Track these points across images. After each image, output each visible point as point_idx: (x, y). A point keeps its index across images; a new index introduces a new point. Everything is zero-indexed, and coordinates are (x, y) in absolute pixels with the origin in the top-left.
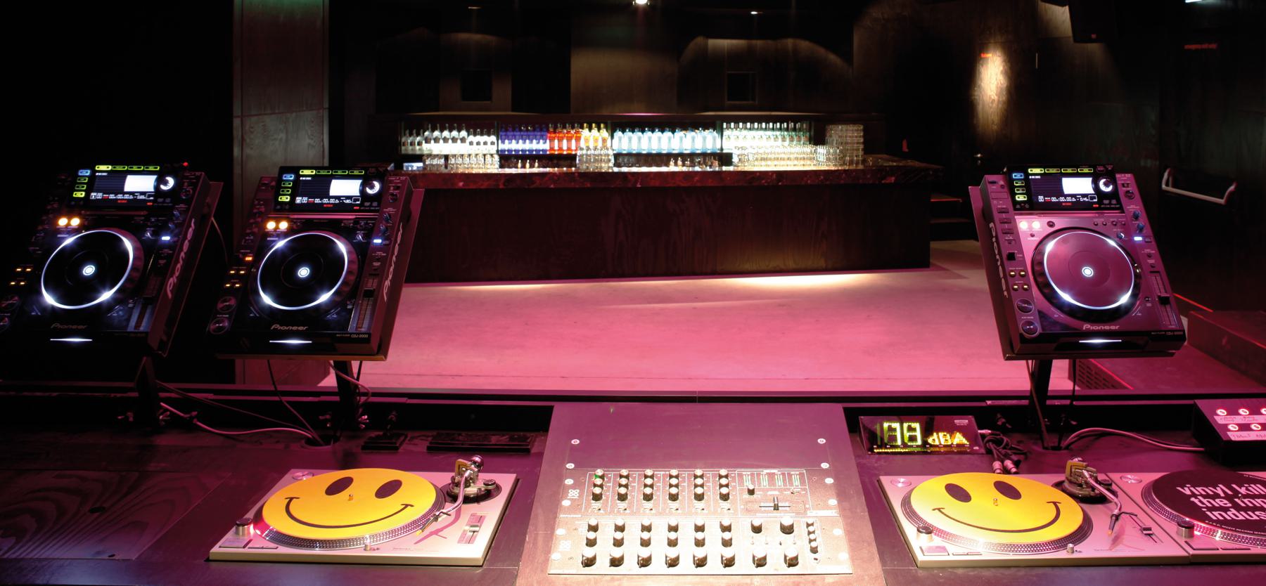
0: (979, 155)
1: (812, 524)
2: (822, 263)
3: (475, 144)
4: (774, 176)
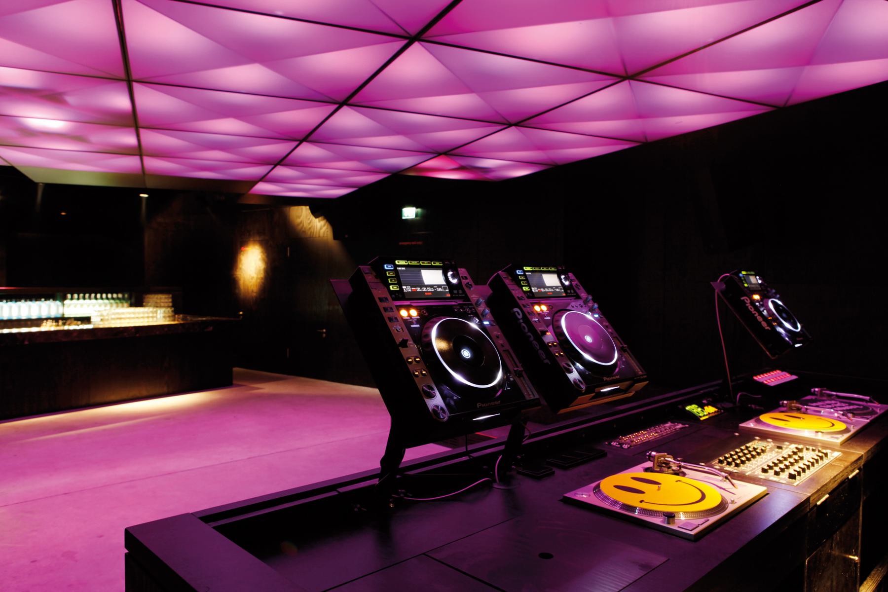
0: (241, 313)
2: (165, 390)
4: (166, 329)
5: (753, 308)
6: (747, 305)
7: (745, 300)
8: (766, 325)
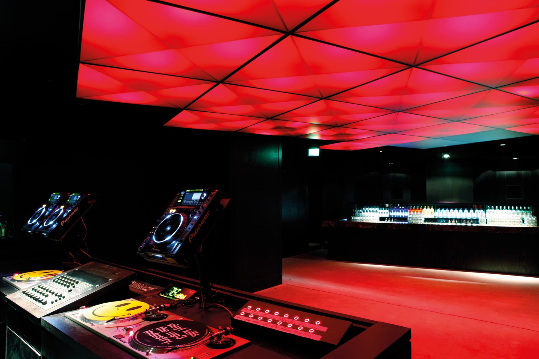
1: (301, 334)
2: (523, 271)
3: (381, 213)
4: (494, 229)
5: (67, 218)
6: (66, 222)
7: (63, 223)
8: (206, 215)
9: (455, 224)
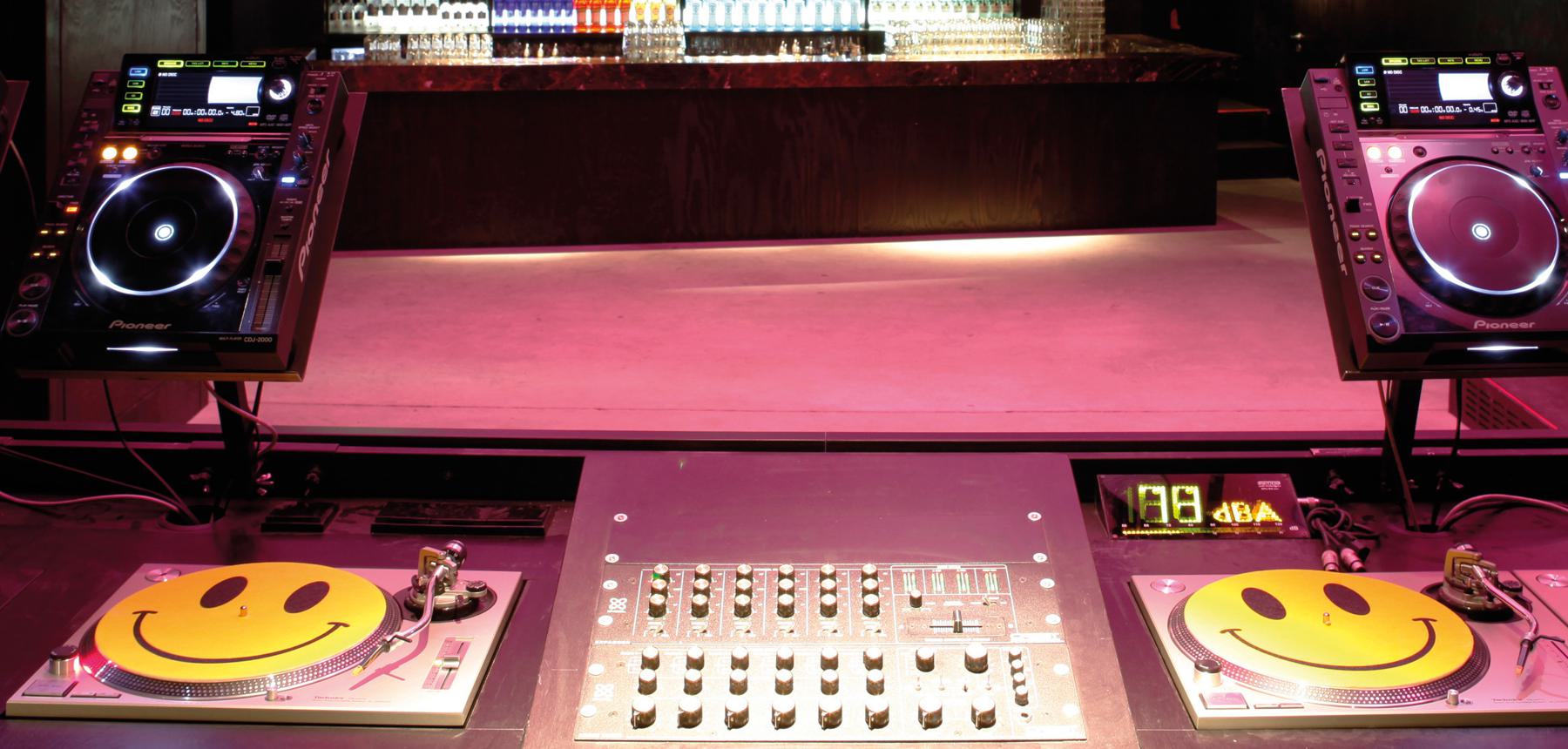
0: (1299, 36)
2: (1034, 217)
8: (162, 325)
9: (804, 59)
